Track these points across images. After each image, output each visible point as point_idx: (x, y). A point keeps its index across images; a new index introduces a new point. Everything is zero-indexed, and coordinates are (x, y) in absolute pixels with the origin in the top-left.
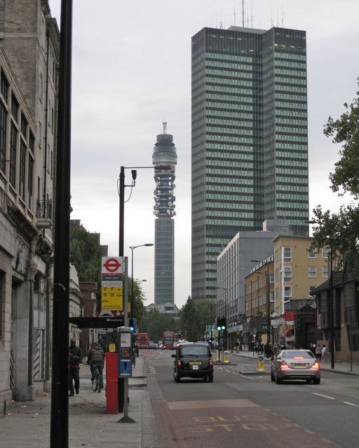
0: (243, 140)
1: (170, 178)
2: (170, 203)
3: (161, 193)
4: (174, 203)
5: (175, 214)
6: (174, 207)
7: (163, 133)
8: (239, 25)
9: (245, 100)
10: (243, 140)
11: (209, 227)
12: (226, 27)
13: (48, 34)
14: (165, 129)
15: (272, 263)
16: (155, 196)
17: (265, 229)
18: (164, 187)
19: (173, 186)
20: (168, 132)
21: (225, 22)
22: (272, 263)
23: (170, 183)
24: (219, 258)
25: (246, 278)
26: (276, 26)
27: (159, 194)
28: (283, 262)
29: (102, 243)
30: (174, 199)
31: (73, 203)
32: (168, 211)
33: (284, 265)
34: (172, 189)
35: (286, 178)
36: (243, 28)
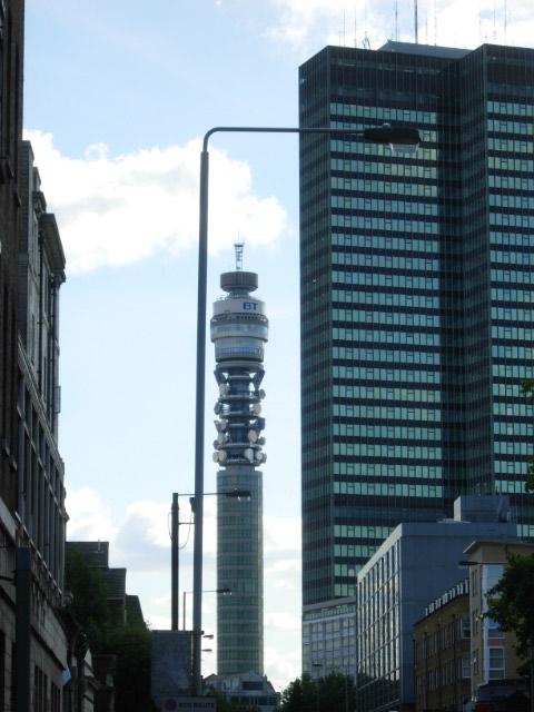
0: (418, 434)
1: (252, 375)
2: (252, 435)
3: (232, 409)
4: (263, 434)
5: (263, 460)
6: (262, 442)
7: (234, 270)
8: (406, 38)
9: (420, 209)
10: (418, 434)
11: (342, 500)
12: (376, 46)
13: (41, 242)
14: (238, 258)
15: (465, 596)
16: (218, 418)
17: (458, 517)
18: (239, 396)
19: (259, 395)
20: (246, 268)
21: (370, 35)
22: (465, 596)
23: (252, 387)
24: (361, 574)
25: (415, 625)
26: (491, 42)
27: (226, 414)
28: (485, 634)
29: (130, 590)
30: (260, 424)
31: (70, 505)
32: (249, 454)
33: (490, 643)
34: (256, 401)
35: (513, 254)
36: (416, 46)
